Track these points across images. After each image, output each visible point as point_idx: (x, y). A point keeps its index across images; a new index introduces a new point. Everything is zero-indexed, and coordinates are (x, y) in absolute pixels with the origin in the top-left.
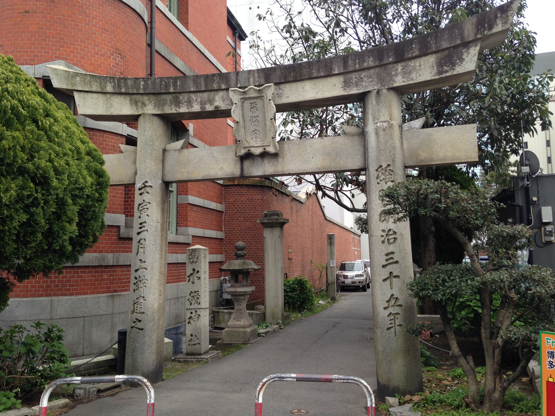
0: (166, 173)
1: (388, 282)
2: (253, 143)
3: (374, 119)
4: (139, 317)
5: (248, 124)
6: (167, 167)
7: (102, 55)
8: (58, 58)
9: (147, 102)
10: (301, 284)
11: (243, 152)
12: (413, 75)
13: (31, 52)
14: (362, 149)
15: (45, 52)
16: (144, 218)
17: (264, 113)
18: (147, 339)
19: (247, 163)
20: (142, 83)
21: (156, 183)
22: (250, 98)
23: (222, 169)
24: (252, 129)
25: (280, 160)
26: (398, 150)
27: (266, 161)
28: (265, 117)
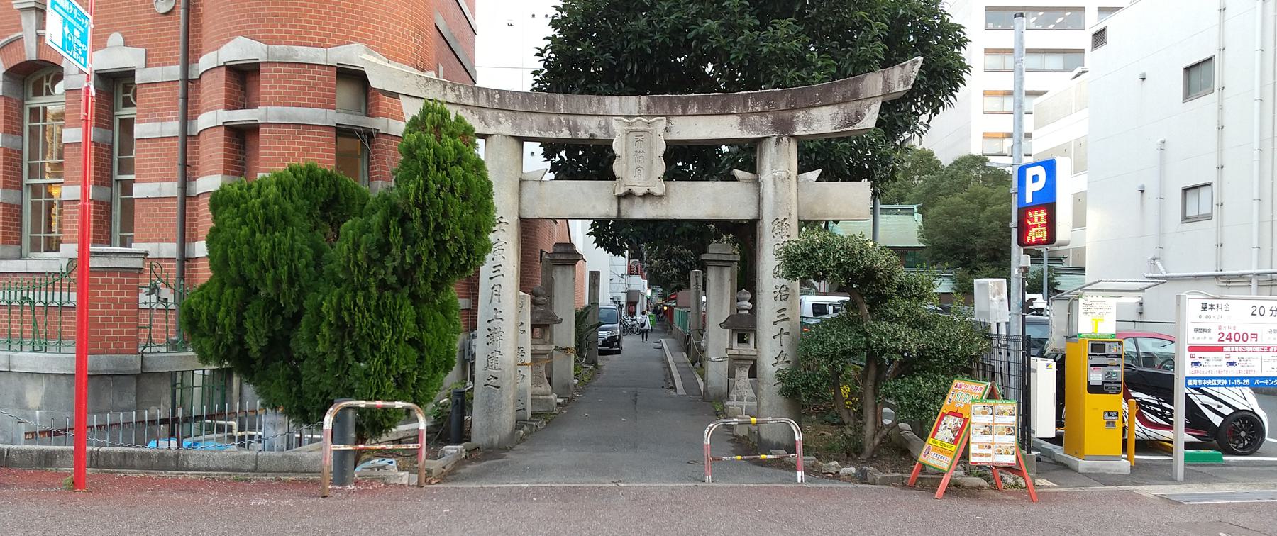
0: (523, 207)
1: (778, 339)
2: (635, 181)
3: (772, 168)
4: (495, 373)
5: (632, 159)
6: (524, 202)
7: (404, 36)
8: (355, 40)
9: (502, 120)
10: (863, 283)
11: (622, 191)
12: (814, 126)
13: (321, 29)
14: (756, 198)
15: (340, 31)
16: (499, 260)
17: (651, 149)
18: (504, 398)
19: (624, 203)
20: (498, 96)
21: (513, 220)
22: (636, 131)
23: (594, 207)
24: (635, 165)
25: (665, 203)
26: (795, 202)
27: (648, 202)
28: (651, 154)
